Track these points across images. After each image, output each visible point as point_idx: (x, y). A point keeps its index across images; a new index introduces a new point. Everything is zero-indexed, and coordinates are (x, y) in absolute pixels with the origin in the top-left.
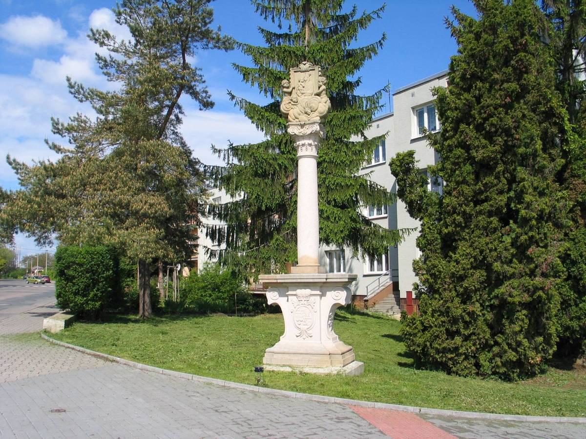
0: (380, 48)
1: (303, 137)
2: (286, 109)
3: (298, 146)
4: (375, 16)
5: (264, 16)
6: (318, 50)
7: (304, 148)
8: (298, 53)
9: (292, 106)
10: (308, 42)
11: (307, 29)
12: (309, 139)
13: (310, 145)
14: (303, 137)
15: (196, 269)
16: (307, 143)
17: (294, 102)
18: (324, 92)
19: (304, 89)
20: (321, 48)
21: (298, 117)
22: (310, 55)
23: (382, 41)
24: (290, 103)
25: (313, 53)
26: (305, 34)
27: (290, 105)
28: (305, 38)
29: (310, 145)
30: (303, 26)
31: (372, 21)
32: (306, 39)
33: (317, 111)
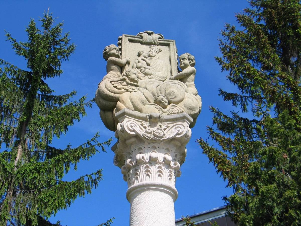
0: (94, 187)
1: (155, 143)
2: (115, 90)
3: (139, 163)
4: (100, 149)
5: (53, 26)
6: (31, 171)
7: (154, 169)
8: (8, 168)
9: (128, 87)
10: (18, 162)
11: (20, 150)
12: (167, 151)
13: (167, 163)
14: (155, 143)
15: (180, 162)
16: (161, 159)
17: (132, 80)
18: (192, 76)
19: (148, 67)
20: (35, 169)
21: (141, 106)
22: (19, 175)
23: (97, 180)
24: (124, 80)
25: (24, 173)
26: (16, 154)
27: (124, 83)
28: (15, 158)
29: (167, 163)
30: (15, 146)
31: (96, 153)
32: (17, 159)
33: (181, 104)
